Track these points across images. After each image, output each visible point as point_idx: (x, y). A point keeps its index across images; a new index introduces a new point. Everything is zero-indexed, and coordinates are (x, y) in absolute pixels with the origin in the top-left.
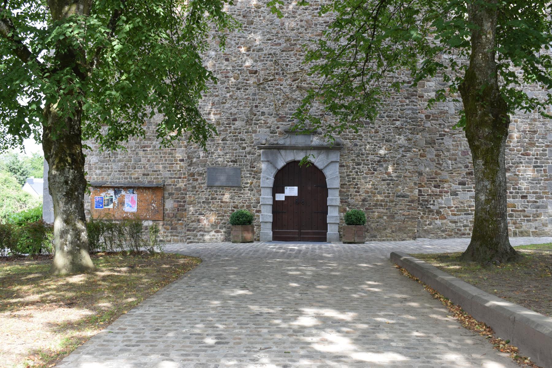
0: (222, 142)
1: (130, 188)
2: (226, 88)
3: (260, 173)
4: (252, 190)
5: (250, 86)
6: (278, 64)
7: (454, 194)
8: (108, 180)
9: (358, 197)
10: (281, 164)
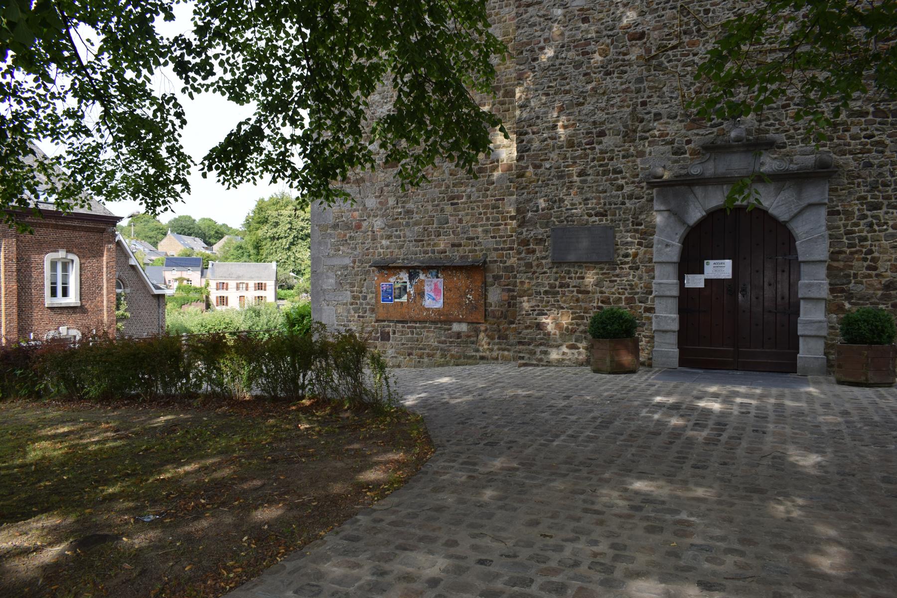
0: (578, 179)
1: (432, 268)
2: (585, 75)
3: (652, 235)
4: (637, 268)
5: (630, 65)
6: (689, 13)
8: (400, 255)
9: (874, 281)
10: (695, 214)
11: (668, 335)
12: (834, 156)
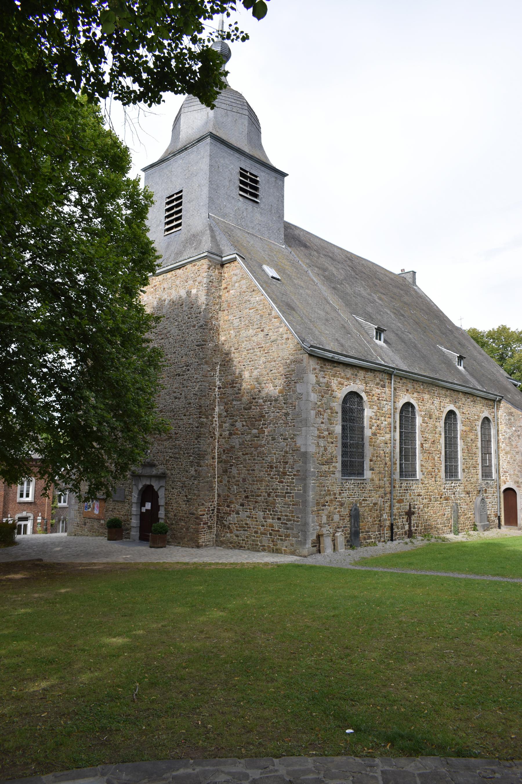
7: (238, 513)
10: (140, 487)
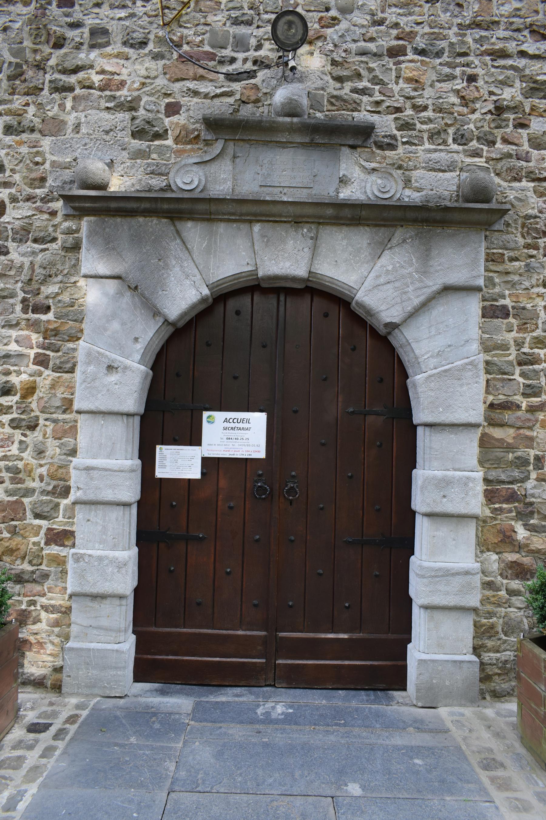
4: (33, 427)
11: (106, 607)
12: (497, 180)
